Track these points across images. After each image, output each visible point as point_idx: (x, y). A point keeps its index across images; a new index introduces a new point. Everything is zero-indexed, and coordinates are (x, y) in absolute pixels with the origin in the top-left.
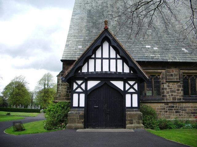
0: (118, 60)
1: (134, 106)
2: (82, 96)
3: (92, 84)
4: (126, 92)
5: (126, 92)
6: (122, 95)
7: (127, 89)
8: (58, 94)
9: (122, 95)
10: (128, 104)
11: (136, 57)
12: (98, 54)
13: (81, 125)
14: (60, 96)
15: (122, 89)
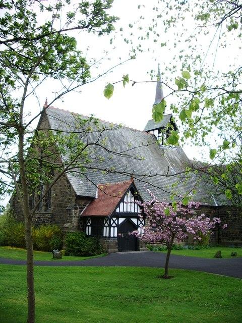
2: (116, 229)
3: (121, 220)
8: (72, 225)
12: (125, 200)
13: (116, 250)
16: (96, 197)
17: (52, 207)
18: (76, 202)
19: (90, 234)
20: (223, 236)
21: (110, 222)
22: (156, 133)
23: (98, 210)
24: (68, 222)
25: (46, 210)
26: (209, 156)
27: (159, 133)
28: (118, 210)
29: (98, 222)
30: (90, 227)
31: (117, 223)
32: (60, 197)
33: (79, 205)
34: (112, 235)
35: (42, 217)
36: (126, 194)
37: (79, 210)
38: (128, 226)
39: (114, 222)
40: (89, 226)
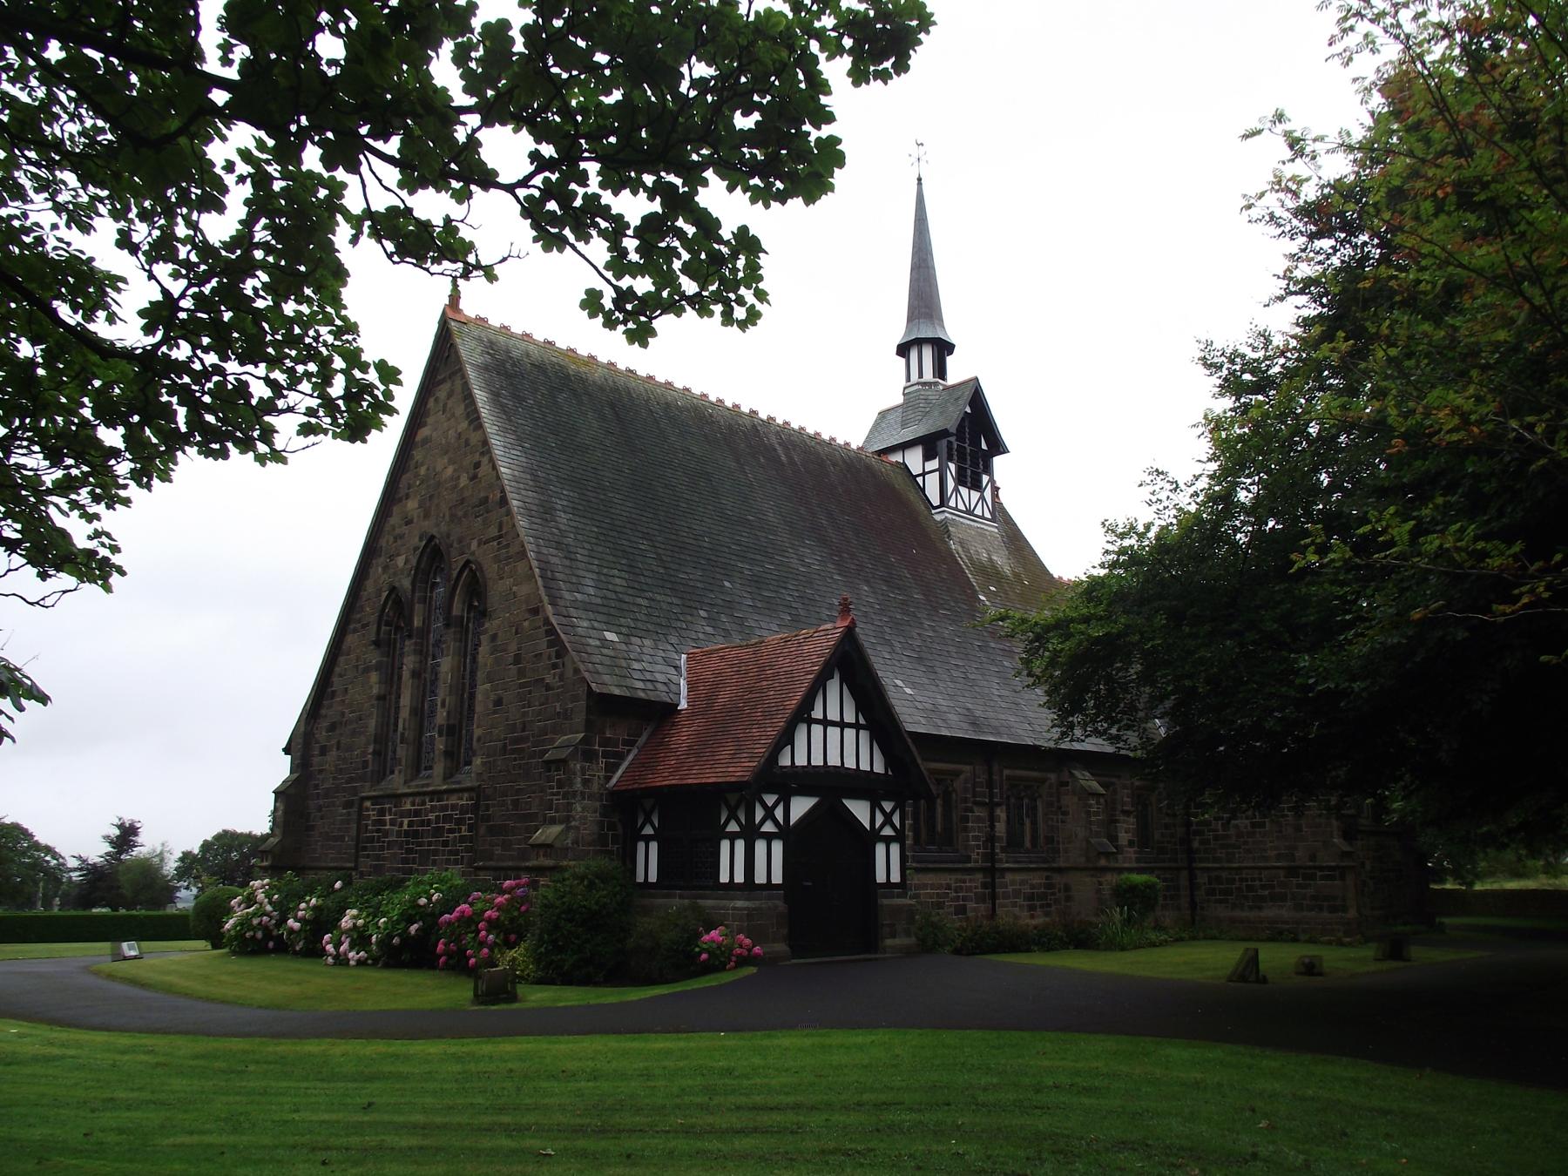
2: (778, 847)
3: (801, 806)
5: (874, 836)
6: (866, 840)
8: (571, 835)
9: (866, 840)
10: (881, 877)
11: (914, 721)
12: (817, 713)
13: (781, 947)
14: (576, 842)
16: (683, 705)
17: (478, 761)
18: (589, 726)
19: (653, 878)
21: (751, 814)
23: (684, 765)
24: (553, 821)
25: (447, 777)
26: (230, 827)
27: (927, 457)
28: (785, 761)
29: (692, 820)
30: (654, 846)
34: (760, 878)
35: (433, 809)
36: (819, 685)
37: (602, 762)
38: (827, 849)
40: (647, 839)
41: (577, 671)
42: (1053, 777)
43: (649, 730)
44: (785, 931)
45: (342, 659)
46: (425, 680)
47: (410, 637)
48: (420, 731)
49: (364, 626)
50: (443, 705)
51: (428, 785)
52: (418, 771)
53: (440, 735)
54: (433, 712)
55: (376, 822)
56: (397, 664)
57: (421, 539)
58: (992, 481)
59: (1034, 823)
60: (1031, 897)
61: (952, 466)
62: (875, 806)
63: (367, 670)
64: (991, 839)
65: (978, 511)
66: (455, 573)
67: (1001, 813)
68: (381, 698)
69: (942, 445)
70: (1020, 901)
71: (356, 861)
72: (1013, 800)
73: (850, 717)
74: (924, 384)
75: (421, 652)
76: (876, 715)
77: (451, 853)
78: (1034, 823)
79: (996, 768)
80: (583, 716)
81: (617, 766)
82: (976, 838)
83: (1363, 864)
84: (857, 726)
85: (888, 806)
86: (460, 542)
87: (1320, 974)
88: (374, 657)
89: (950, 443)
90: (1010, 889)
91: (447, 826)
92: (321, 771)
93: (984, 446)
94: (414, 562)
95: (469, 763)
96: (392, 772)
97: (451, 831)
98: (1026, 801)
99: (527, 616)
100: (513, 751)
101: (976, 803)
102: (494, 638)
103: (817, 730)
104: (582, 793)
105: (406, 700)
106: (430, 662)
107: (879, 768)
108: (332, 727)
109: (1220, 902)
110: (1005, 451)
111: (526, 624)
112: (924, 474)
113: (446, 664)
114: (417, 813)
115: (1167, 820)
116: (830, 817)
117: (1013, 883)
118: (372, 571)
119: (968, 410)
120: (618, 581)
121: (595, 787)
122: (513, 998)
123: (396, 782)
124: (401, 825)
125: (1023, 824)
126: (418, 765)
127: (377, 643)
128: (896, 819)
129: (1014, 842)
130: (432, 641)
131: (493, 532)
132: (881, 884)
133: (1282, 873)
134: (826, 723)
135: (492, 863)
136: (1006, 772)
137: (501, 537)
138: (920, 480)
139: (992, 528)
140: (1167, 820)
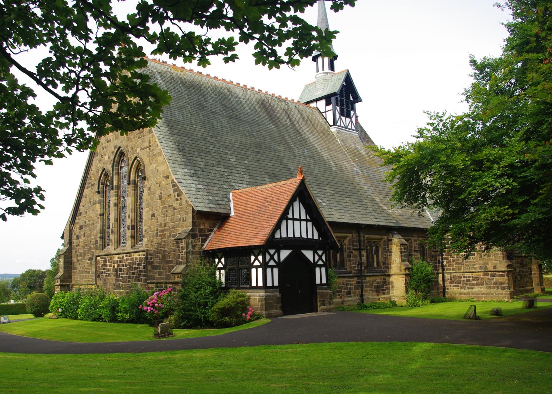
0: (308, 223)
1: (323, 282)
2: (276, 270)
3: (285, 254)
4: (315, 265)
5: (315, 265)
7: (316, 260)
10: (318, 281)
12: (290, 216)
13: (279, 311)
15: (312, 260)
16: (232, 214)
17: (145, 240)
20: (451, 283)
22: (321, 105)
24: (181, 263)
25: (133, 246)
26: (41, 269)
27: (328, 104)
28: (277, 236)
31: (277, 260)
32: (160, 219)
33: (201, 230)
34: (269, 284)
37: (200, 239)
39: (272, 257)
41: (187, 201)
42: (385, 237)
43: (218, 224)
44: (280, 305)
45: (83, 199)
46: (120, 208)
47: (112, 189)
48: (119, 228)
49: (92, 185)
50: (129, 217)
51: (125, 250)
52: (120, 244)
53: (129, 229)
54: (124, 220)
55: (102, 266)
56: (107, 201)
57: (115, 148)
58: (355, 113)
59: (378, 257)
60: (377, 287)
61: (338, 108)
62: (315, 252)
63: (94, 204)
64: (360, 264)
65: (350, 127)
66: (131, 162)
67: (364, 253)
68: (102, 215)
69: (333, 99)
70: (373, 288)
71: (96, 282)
72: (369, 247)
73: (303, 217)
74: (325, 73)
75: (118, 195)
76: (314, 216)
77: (136, 277)
78: (378, 257)
79: (362, 235)
80: (191, 220)
81: (206, 240)
82: (354, 264)
83: (516, 270)
84: (306, 220)
85: (320, 252)
86: (132, 149)
87: (501, 315)
88: (98, 198)
89: (337, 98)
90: (368, 284)
91: (134, 266)
92: (77, 246)
93: (351, 99)
94: (112, 158)
95: (141, 240)
96: (108, 245)
97: (136, 268)
98: (374, 248)
99: (164, 179)
100: (161, 235)
101: (354, 249)
102: (150, 189)
103: (290, 222)
104: (192, 252)
105: (113, 216)
106: (122, 199)
107: (316, 237)
108: (81, 228)
109: (455, 286)
110: (361, 101)
111: (163, 182)
112: (326, 112)
113: (129, 201)
114: (120, 262)
115: (433, 253)
116: (297, 258)
117: (369, 281)
118: (94, 162)
119: (344, 84)
120: (201, 163)
121: (197, 249)
122: (171, 334)
123: (111, 249)
124: (114, 266)
125: (373, 257)
126: (119, 242)
127: (98, 192)
128: (324, 258)
129: (369, 264)
130: (122, 191)
131: (147, 144)
132: (318, 284)
133: (482, 274)
134: (294, 219)
135: (155, 281)
136: (366, 236)
137: (150, 146)
138: (324, 114)
139: (356, 134)
140: (433, 253)
